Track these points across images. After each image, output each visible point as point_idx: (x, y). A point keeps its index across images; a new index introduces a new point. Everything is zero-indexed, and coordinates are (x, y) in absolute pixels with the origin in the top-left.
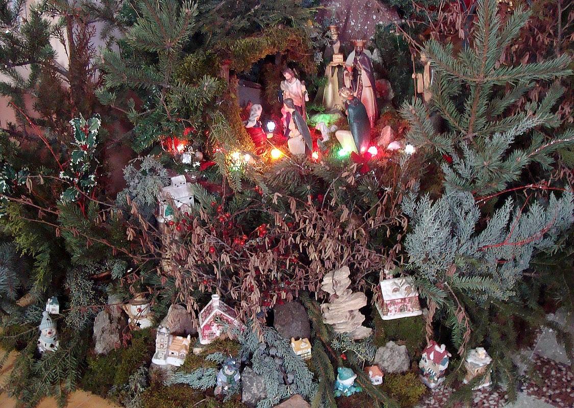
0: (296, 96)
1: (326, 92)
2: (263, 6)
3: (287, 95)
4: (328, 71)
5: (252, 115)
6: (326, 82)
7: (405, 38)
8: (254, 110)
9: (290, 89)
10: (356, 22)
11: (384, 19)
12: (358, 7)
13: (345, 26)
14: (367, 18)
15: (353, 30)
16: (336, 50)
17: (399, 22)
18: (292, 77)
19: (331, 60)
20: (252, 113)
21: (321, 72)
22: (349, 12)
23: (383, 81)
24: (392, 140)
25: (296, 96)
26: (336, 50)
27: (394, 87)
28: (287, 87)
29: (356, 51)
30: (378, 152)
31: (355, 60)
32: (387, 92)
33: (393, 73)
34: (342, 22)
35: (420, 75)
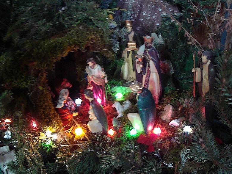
0: (98, 78)
1: (124, 69)
2: (69, 8)
3: (90, 79)
4: (125, 54)
5: (61, 98)
6: (123, 62)
7: (186, 35)
8: (62, 94)
9: (93, 73)
10: (147, 13)
11: (167, 12)
12: (148, 3)
13: (139, 16)
14: (155, 10)
15: (144, 19)
16: (131, 39)
17: (179, 14)
18: (94, 64)
19: (127, 46)
20: (60, 97)
21: (119, 55)
22: (141, 6)
23: (165, 62)
24: (173, 118)
25: (98, 78)
26: (131, 39)
27: (174, 66)
28: (91, 71)
29: (145, 45)
30: (162, 131)
31: (145, 51)
32: (169, 70)
33: (173, 59)
34: (136, 13)
35: (198, 69)
